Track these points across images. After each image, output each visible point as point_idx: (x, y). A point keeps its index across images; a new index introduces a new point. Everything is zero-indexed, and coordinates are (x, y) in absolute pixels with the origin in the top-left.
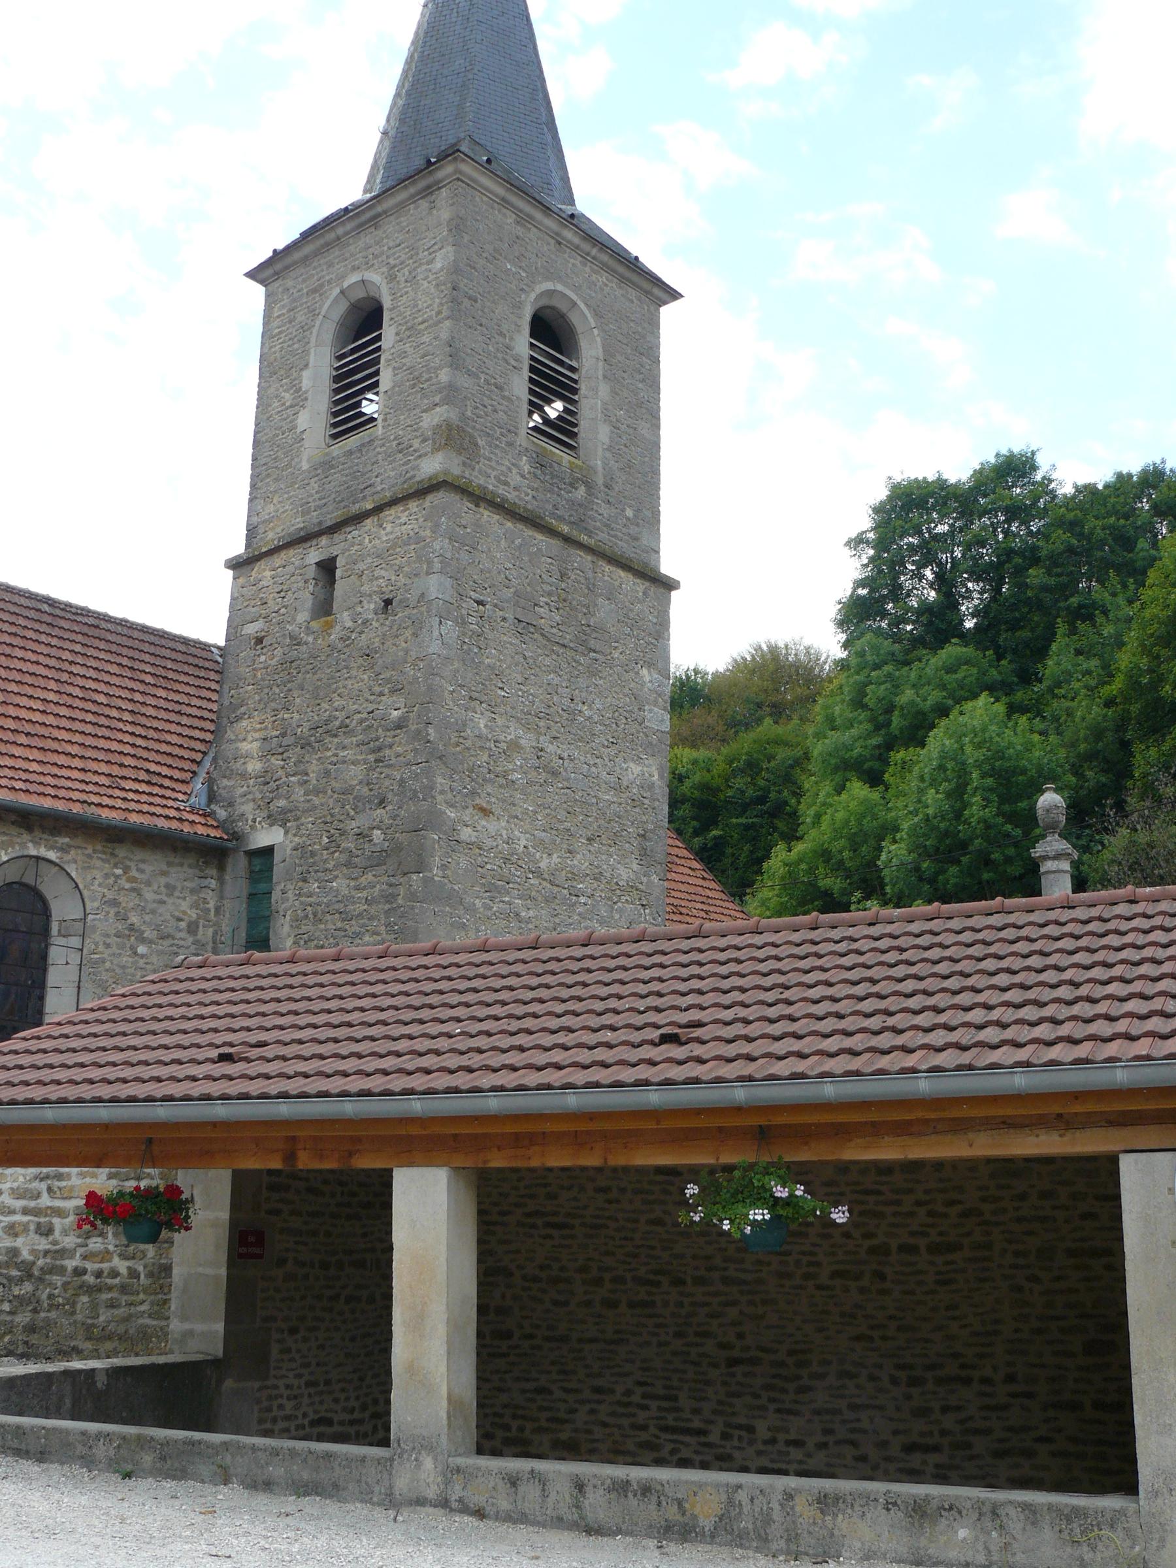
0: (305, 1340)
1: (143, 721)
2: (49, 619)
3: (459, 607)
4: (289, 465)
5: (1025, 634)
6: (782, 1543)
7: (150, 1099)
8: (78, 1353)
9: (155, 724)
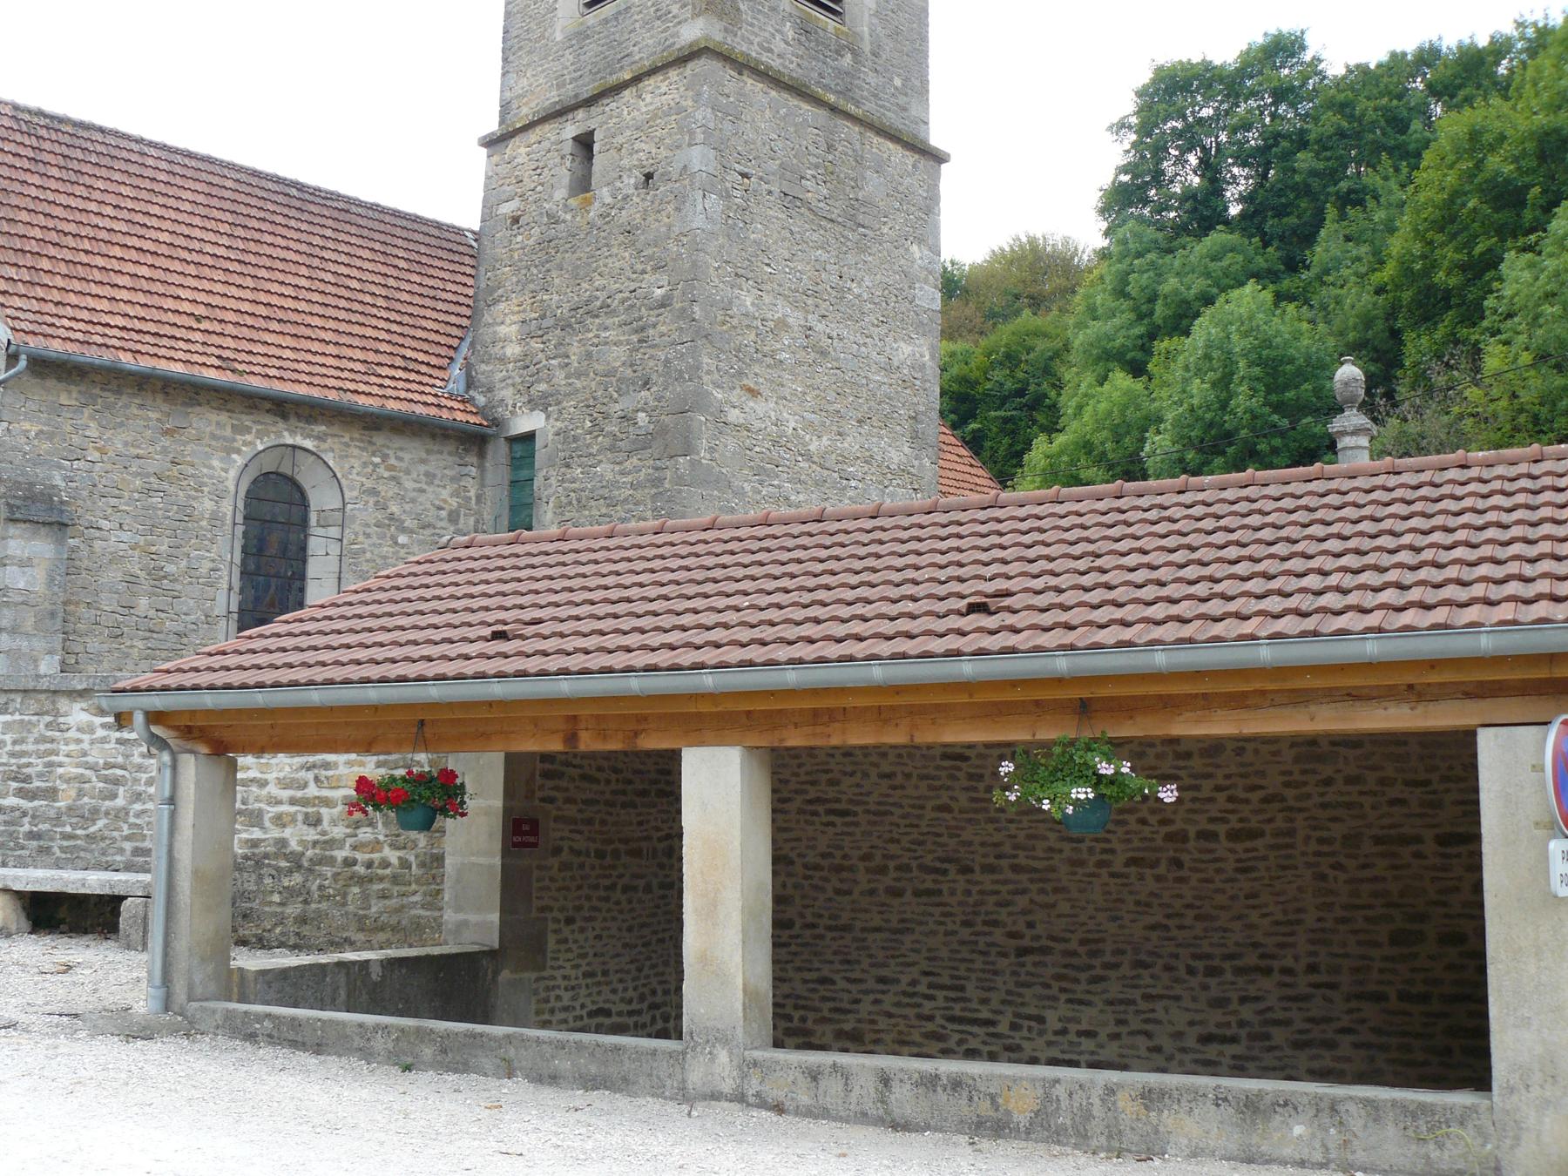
0: (582, 930)
1: (398, 306)
2: (298, 204)
3: (723, 180)
4: (542, 36)
5: (1292, 220)
6: (1103, 1139)
7: (421, 679)
8: (350, 944)
9: (410, 309)
